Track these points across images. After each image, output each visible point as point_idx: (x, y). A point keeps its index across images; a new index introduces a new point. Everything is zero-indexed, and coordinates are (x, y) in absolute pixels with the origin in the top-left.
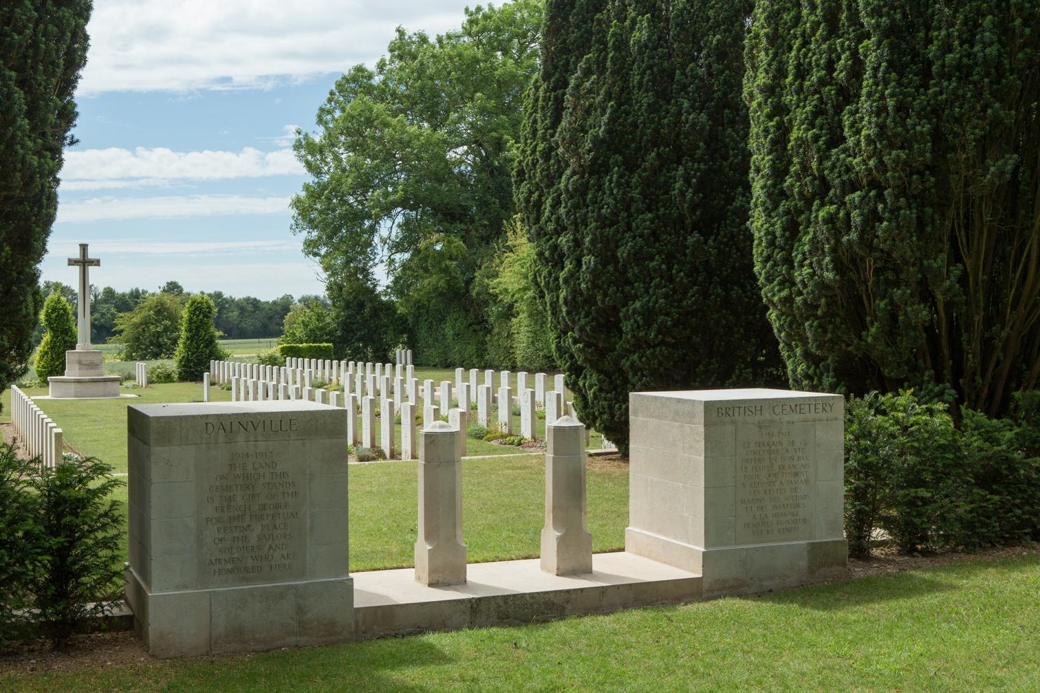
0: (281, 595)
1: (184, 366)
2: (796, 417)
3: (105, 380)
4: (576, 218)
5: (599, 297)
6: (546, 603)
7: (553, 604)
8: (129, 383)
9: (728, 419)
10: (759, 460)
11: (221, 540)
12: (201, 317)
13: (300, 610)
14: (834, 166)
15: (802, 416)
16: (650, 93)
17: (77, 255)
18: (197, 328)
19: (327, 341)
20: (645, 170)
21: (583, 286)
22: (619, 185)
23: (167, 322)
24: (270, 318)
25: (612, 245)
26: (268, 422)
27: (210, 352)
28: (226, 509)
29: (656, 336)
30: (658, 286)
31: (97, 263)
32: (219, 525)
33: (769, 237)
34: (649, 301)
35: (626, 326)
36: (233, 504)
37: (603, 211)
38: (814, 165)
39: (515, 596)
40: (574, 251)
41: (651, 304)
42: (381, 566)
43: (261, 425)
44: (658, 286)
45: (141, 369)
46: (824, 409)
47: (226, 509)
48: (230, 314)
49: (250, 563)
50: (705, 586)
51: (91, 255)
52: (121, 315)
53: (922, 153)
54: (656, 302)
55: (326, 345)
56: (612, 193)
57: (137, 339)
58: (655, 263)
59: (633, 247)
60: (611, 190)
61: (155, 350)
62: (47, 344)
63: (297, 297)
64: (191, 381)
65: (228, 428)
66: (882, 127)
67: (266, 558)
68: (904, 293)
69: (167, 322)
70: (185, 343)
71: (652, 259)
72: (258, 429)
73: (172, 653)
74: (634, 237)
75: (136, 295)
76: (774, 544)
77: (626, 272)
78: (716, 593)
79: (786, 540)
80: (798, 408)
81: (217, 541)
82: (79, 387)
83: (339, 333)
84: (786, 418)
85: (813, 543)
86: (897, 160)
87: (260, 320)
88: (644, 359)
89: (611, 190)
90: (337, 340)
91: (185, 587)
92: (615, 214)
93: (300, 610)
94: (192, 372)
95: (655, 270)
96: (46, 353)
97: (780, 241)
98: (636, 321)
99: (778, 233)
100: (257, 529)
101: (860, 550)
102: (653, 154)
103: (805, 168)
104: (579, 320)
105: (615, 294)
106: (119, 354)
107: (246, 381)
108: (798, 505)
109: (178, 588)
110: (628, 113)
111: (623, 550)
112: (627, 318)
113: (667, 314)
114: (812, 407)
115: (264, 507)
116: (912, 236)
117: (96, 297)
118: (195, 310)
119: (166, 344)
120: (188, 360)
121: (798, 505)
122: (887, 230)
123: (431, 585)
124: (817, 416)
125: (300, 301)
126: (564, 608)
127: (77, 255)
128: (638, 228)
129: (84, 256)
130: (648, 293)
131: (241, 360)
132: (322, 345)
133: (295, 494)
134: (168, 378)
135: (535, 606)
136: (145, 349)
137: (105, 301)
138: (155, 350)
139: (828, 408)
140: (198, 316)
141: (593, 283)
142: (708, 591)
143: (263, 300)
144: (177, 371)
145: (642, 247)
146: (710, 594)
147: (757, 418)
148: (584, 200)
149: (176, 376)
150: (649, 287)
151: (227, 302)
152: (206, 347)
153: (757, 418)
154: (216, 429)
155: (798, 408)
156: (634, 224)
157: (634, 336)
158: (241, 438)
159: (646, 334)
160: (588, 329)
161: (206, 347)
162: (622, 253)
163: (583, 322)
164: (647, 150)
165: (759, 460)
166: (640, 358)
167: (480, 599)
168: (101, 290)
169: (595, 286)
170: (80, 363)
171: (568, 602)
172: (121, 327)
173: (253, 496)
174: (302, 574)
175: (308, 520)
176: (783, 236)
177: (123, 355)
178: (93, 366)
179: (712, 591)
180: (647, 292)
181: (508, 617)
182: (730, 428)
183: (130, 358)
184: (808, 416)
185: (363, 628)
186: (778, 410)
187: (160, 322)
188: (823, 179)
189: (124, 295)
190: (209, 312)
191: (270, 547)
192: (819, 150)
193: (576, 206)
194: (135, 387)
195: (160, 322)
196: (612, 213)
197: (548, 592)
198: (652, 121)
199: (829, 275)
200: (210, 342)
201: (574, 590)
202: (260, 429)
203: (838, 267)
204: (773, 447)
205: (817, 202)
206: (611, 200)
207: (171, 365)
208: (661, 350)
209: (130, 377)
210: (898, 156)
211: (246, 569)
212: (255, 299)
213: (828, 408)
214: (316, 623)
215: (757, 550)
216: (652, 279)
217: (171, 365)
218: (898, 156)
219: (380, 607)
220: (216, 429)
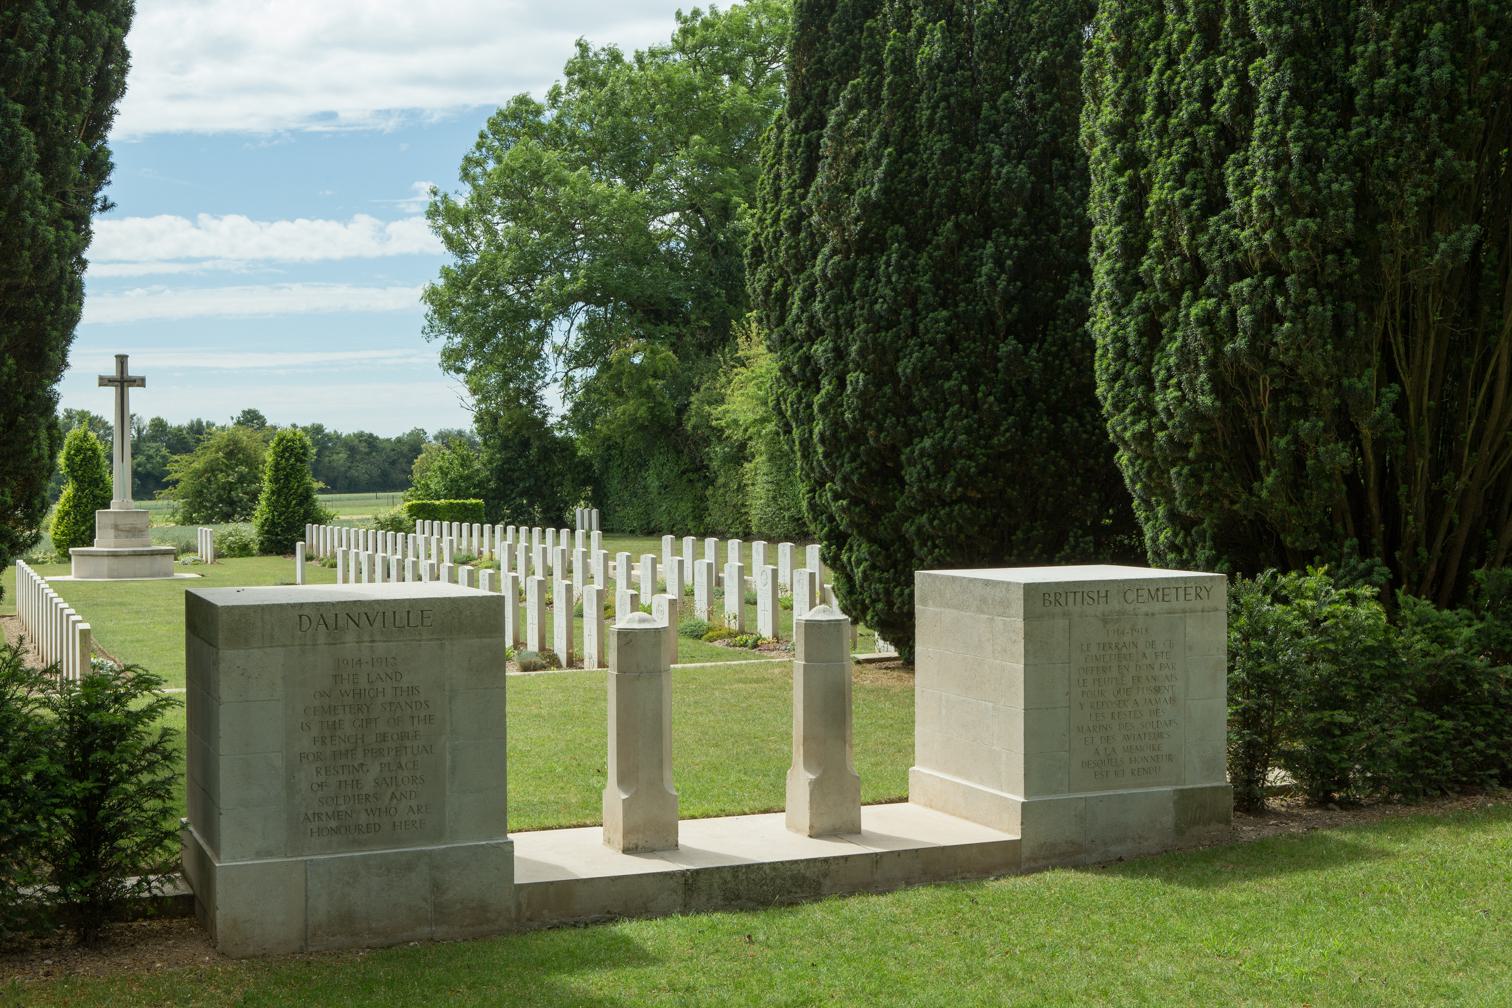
0: (409, 865)
1: (267, 532)
2: (1158, 606)
3: (153, 553)
4: (837, 317)
5: (871, 433)
8: (188, 558)
9: (1058, 609)
11: (321, 785)
12: (292, 461)
13: (437, 887)
14: (1212, 242)
15: (1166, 606)
16: (946, 136)
17: (112, 370)
18: (287, 477)
19: (475, 496)
20: (938, 247)
22: (900, 269)
23: (244, 469)
24: (393, 463)
25: (890, 357)
26: (389, 614)
27: (306, 512)
28: (328, 740)
29: (954, 489)
30: (957, 416)
31: (140, 382)
33: (1118, 345)
34: (943, 438)
35: (911, 474)
36: (339, 733)
37: (877, 307)
38: (1184, 240)
39: (748, 866)
40: (835, 365)
41: (946, 443)
43: (379, 618)
44: (957, 416)
45: (205, 537)
46: (1197, 595)
47: (328, 740)
48: (335, 457)
49: (363, 819)
50: (1026, 852)
51: (133, 370)
52: (176, 457)
54: (954, 439)
55: (474, 501)
56: (889, 281)
57: (199, 493)
58: (952, 383)
59: (920, 360)
60: (889, 277)
61: (225, 509)
62: (68, 500)
63: (431, 432)
64: (278, 554)
65: (331, 622)
66: (1282, 185)
67: (387, 811)
69: (244, 469)
70: (268, 499)
71: (948, 377)
72: (376, 625)
74: (922, 345)
75: (198, 429)
77: (910, 395)
78: (1042, 862)
79: (1141, 786)
80: (1160, 593)
81: (315, 787)
83: (492, 485)
84: (1144, 608)
85: (1181, 791)
86: (1304, 234)
87: (378, 465)
88: (936, 523)
90: (491, 495)
91: (269, 854)
92: (895, 311)
93: (437, 887)
94: (280, 542)
95: (953, 393)
96: (67, 513)
97: (1133, 351)
98: (924, 467)
99: (1131, 339)
100: (374, 770)
101: (1250, 800)
102: (950, 224)
103: (1170, 244)
104: (842, 465)
105: (894, 427)
106: (173, 515)
108: (1160, 735)
109: (259, 855)
110: (913, 165)
111: (905, 800)
112: (912, 462)
113: (970, 457)
114: (1181, 593)
115: (383, 737)
117: (139, 432)
118: (283, 451)
119: (241, 500)
120: (273, 524)
121: (1160, 735)
123: (626, 851)
124: (1189, 605)
125: (436, 438)
127: (112, 370)
128: (927, 331)
131: (350, 523)
132: (468, 502)
133: (429, 719)
134: (244, 550)
135: (778, 881)
136: (211, 508)
137: (153, 438)
138: (225, 509)
140: (287, 460)
141: (862, 411)
143: (382, 436)
144: (258, 539)
145: (933, 360)
146: (1033, 864)
148: (850, 292)
149: (255, 547)
150: (945, 417)
151: (330, 440)
152: (300, 504)
154: (314, 624)
155: (1160, 593)
156: (921, 326)
157: (921, 489)
158: (350, 637)
160: (855, 478)
161: (300, 504)
162: (904, 368)
163: (847, 468)
164: (941, 218)
166: (931, 521)
167: (697, 872)
168: (147, 422)
169: (864, 415)
170: (116, 527)
171: (825, 875)
172: (176, 476)
174: (438, 835)
175: (448, 757)
176: (1138, 343)
177: (178, 517)
178: (135, 532)
180: (940, 424)
181: (738, 897)
183: (188, 520)
186: (1131, 596)
187: (233, 469)
188: (1196, 261)
189: (180, 429)
190: (304, 454)
192: (1190, 219)
193: (838, 300)
194: (196, 563)
195: (233, 469)
196: (890, 310)
197: (796, 862)
199: (1205, 400)
200: (306, 497)
201: (835, 858)
202: (378, 624)
203: (1219, 388)
204: (1124, 650)
205: (1187, 294)
207: (249, 530)
208: (960, 509)
209: (189, 549)
210: (1306, 227)
211: (358, 828)
212: (371, 435)
213: (1203, 593)
214: (459, 906)
215: (1101, 799)
216: (948, 406)
217: (249, 530)
218: (1306, 227)
219: (552, 883)
220: (314, 624)
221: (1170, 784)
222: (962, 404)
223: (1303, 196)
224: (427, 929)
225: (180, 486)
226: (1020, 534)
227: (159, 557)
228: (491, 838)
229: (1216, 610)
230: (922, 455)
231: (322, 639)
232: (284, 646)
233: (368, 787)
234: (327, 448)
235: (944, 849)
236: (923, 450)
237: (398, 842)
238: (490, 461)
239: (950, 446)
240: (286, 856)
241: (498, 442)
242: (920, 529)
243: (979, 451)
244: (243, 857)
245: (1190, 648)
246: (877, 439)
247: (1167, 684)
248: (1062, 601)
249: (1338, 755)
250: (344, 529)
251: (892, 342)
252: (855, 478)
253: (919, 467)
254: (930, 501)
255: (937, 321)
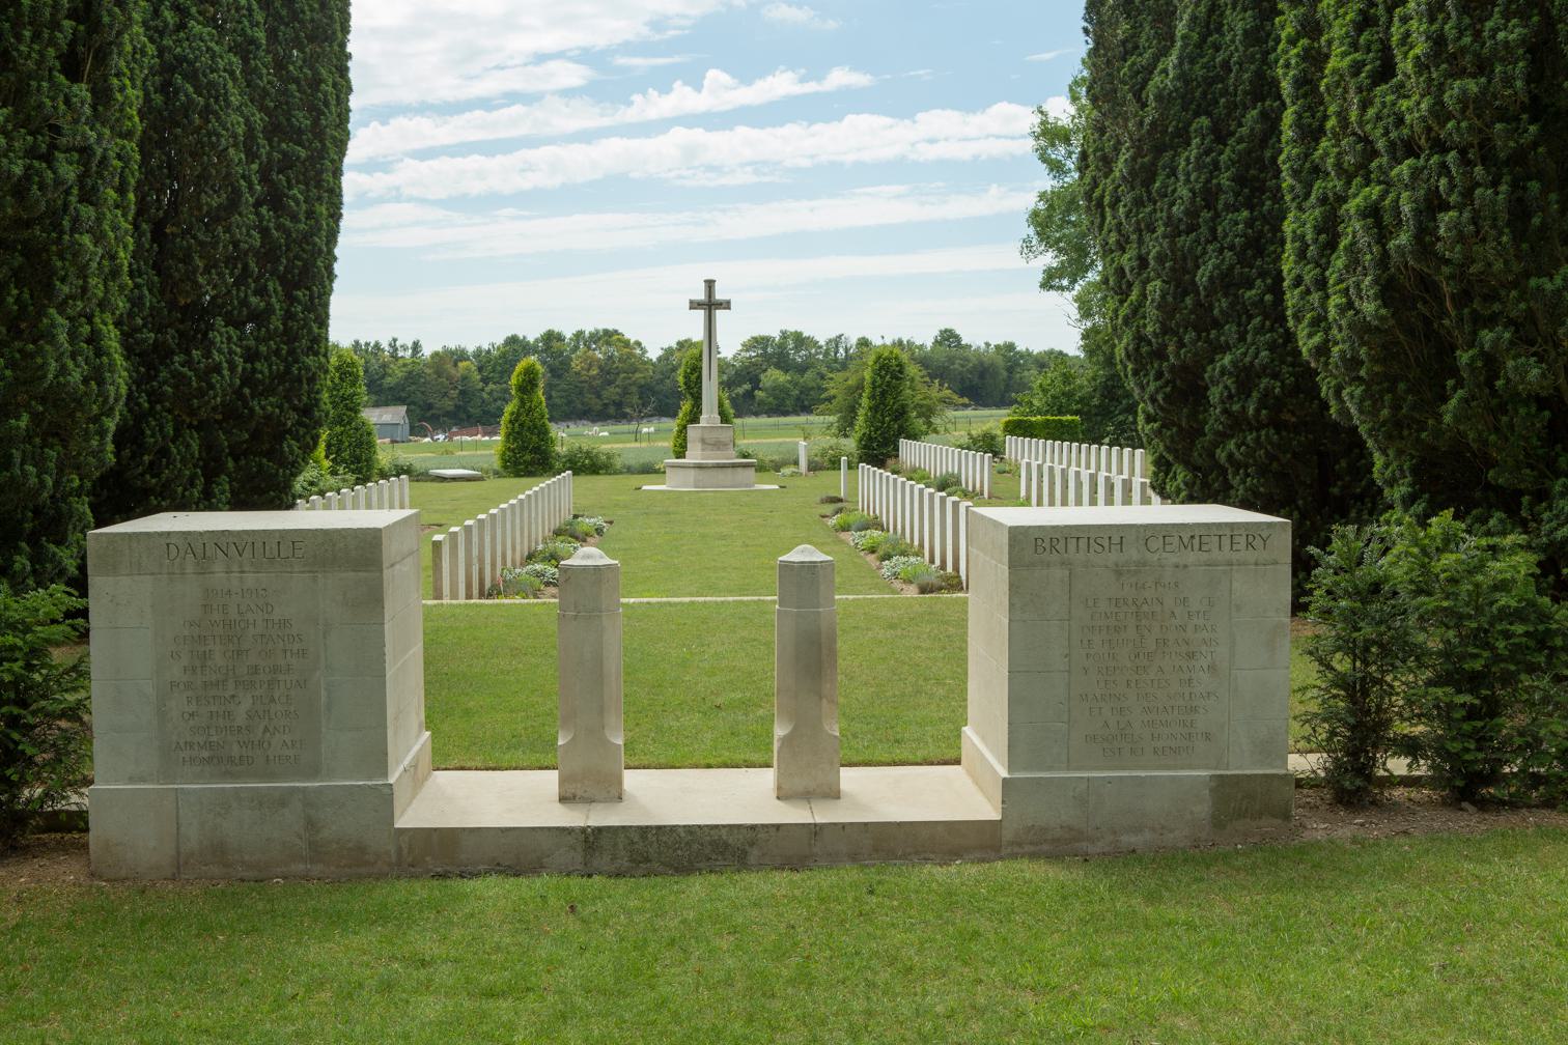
0: (283, 800)
1: (865, 447)
2: (1191, 557)
4: (1138, 223)
5: (1171, 349)
6: (713, 843)
7: (726, 845)
9: (1055, 557)
10: (1117, 629)
11: (192, 715)
12: (888, 378)
13: (311, 825)
14: (1379, 118)
15: (1204, 556)
16: (1249, 13)
17: (701, 296)
18: (883, 393)
19: (1076, 413)
20: (1240, 141)
21: (1149, 329)
22: (1199, 167)
25: (1190, 264)
26: (258, 545)
27: (901, 427)
28: (199, 670)
29: (1258, 411)
30: (1260, 330)
31: (726, 305)
32: (190, 693)
33: (1297, 244)
34: (1245, 354)
35: (1215, 394)
36: (209, 663)
37: (1175, 209)
38: (1353, 115)
39: (659, 828)
40: (1139, 274)
41: (1248, 359)
42: (886, 757)
43: (249, 549)
44: (1260, 330)
46: (1249, 544)
47: (199, 670)
48: (1026, 373)
49: (236, 751)
50: (1007, 835)
51: (719, 296)
52: (831, 375)
53: (1508, 81)
54: (1256, 356)
55: (1069, 417)
56: (1188, 181)
58: (1254, 292)
59: (1216, 267)
60: (1188, 175)
65: (199, 551)
66: (1438, 41)
67: (260, 743)
68: (1499, 338)
71: (1251, 286)
72: (245, 555)
73: (123, 873)
74: (1221, 251)
76: (1143, 774)
77: (1211, 307)
78: (1029, 848)
79: (1168, 768)
80: (1196, 541)
81: (186, 716)
82: (702, 474)
83: (1095, 401)
84: (1173, 559)
85: (1221, 776)
86: (1463, 100)
87: (983, 378)
88: (1243, 448)
89: (1188, 175)
90: (1094, 411)
91: (143, 780)
92: (1192, 213)
93: (311, 825)
95: (1254, 304)
97: (1312, 251)
98: (1226, 387)
99: (1309, 237)
100: (246, 703)
101: (1352, 787)
102: (1254, 113)
103: (1344, 121)
104: (1148, 383)
105: (1194, 342)
107: (1078, 474)
108: (1194, 710)
109: (131, 780)
110: (1217, 48)
111: (957, 762)
112: (1215, 383)
113: (1275, 376)
114: (1226, 541)
115: (255, 670)
116: (1501, 234)
117: (847, 350)
118: (881, 369)
120: (870, 439)
121: (1194, 710)
122: (1455, 225)
123: (563, 799)
124: (1235, 556)
126: (745, 853)
127: (701, 296)
128: (1226, 235)
129: (710, 297)
130: (1245, 340)
132: (1064, 418)
133: (303, 653)
135: (696, 846)
139: (1258, 543)
141: (1163, 324)
142: (1012, 843)
145: (1231, 268)
146: (1016, 849)
147: (1114, 556)
148: (1149, 192)
150: (1246, 332)
151: (1022, 357)
153: (1114, 556)
154: (182, 552)
155: (1196, 541)
156: (1220, 229)
157: (1225, 411)
158: (218, 567)
159: (1243, 407)
160: (1160, 397)
161: (896, 420)
162: (1202, 277)
163: (1152, 387)
164: (1246, 108)
165: (1117, 629)
166: (1238, 447)
167: (599, 830)
168: (853, 341)
169: (1165, 330)
170: (703, 441)
171: (752, 844)
172: (832, 392)
173: (239, 653)
174: (314, 772)
175: (323, 693)
176: (1315, 241)
179: (1020, 845)
180: (1242, 338)
181: (647, 860)
182: (1059, 573)
184: (1216, 554)
185: (410, 859)
186: (1155, 544)
188: (1365, 140)
190: (901, 372)
191: (266, 729)
192: (1360, 90)
193: (1138, 203)
196: (1187, 212)
197: (717, 827)
198: (1252, 59)
199: (1369, 307)
201: (762, 825)
202: (247, 554)
203: (1388, 291)
204: (1145, 608)
205: (1358, 180)
206: (1185, 192)
208: (1267, 435)
210: (1464, 91)
211: (231, 760)
212: (1061, 353)
213: (1258, 543)
214: (335, 846)
215: (1110, 781)
216: (1250, 317)
218: (1464, 91)
219: (436, 829)
220: (182, 552)
221: (1207, 767)
222: (1266, 317)
223: (1463, 50)
224: (301, 866)
225: (834, 402)
226: (1343, 463)
227: (739, 470)
228: (370, 779)
229: (1276, 563)
230: (1222, 373)
231: (190, 569)
232: (152, 574)
233: (240, 719)
234: (1020, 365)
235: (900, 824)
236: (1223, 368)
237: (272, 777)
238: (1094, 379)
239: (1251, 363)
240: (158, 783)
241: (1101, 358)
242: (1230, 456)
243: (1285, 369)
244: (116, 781)
245: (1238, 608)
246: (1177, 355)
247: (1204, 648)
248: (1060, 546)
249: (1480, 737)
250: (1263, 432)
251: (1191, 249)
252: (1160, 397)
253: (1221, 386)
254: (1236, 424)
255: (1237, 223)
